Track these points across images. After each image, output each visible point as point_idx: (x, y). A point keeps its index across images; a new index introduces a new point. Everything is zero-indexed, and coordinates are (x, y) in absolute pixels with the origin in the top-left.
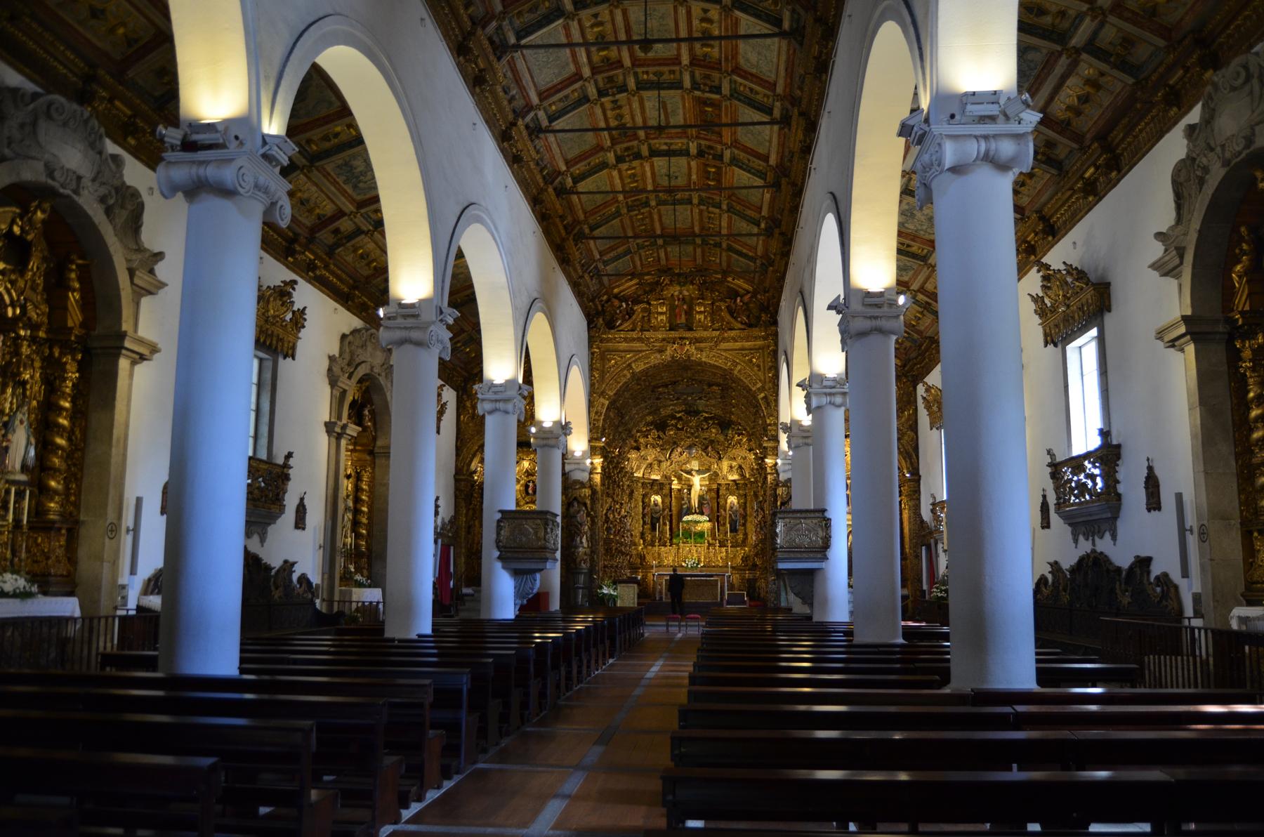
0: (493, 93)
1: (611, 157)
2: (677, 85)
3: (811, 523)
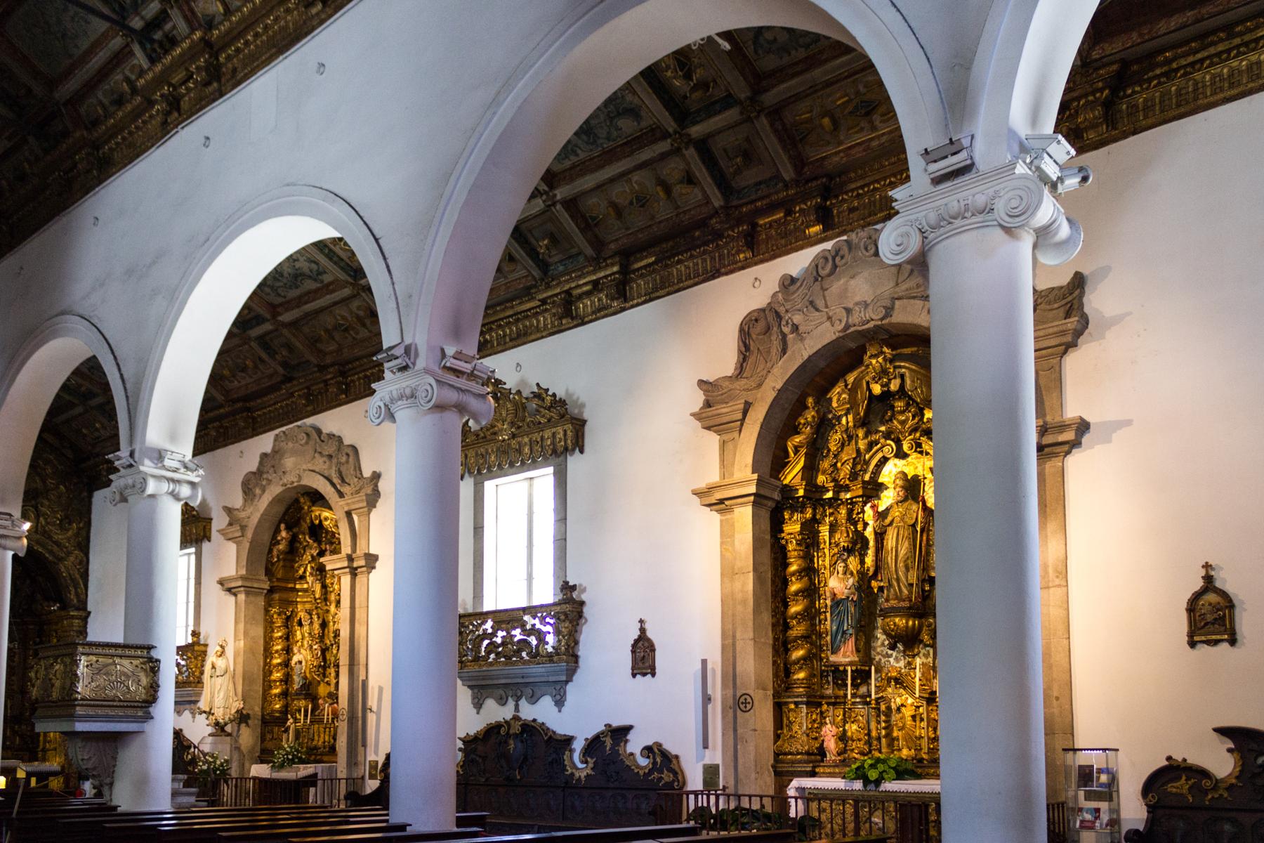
3: (125, 665)
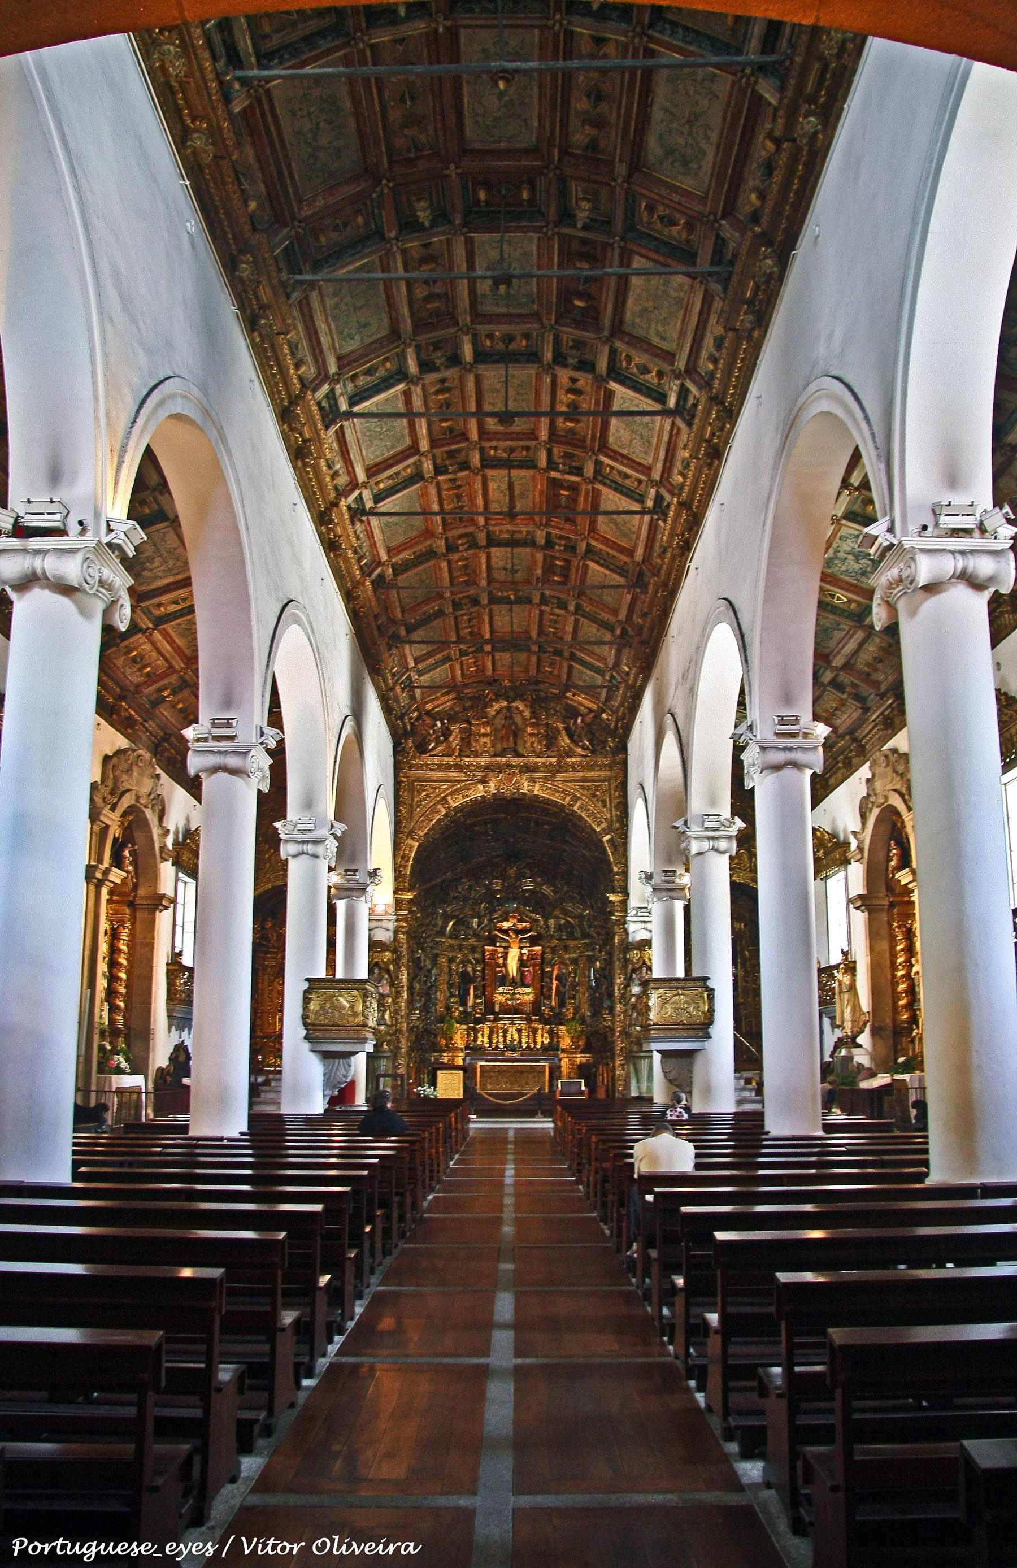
0: (316, 468)
1: (441, 545)
2: (530, 464)
